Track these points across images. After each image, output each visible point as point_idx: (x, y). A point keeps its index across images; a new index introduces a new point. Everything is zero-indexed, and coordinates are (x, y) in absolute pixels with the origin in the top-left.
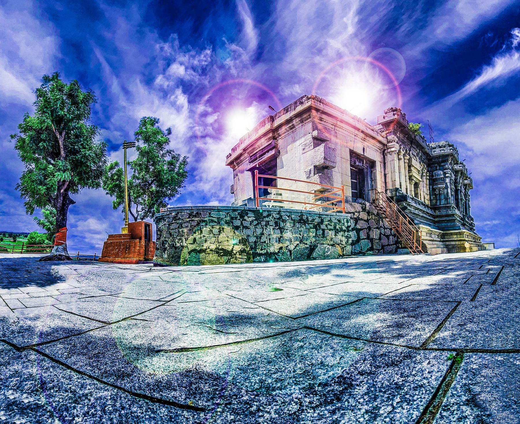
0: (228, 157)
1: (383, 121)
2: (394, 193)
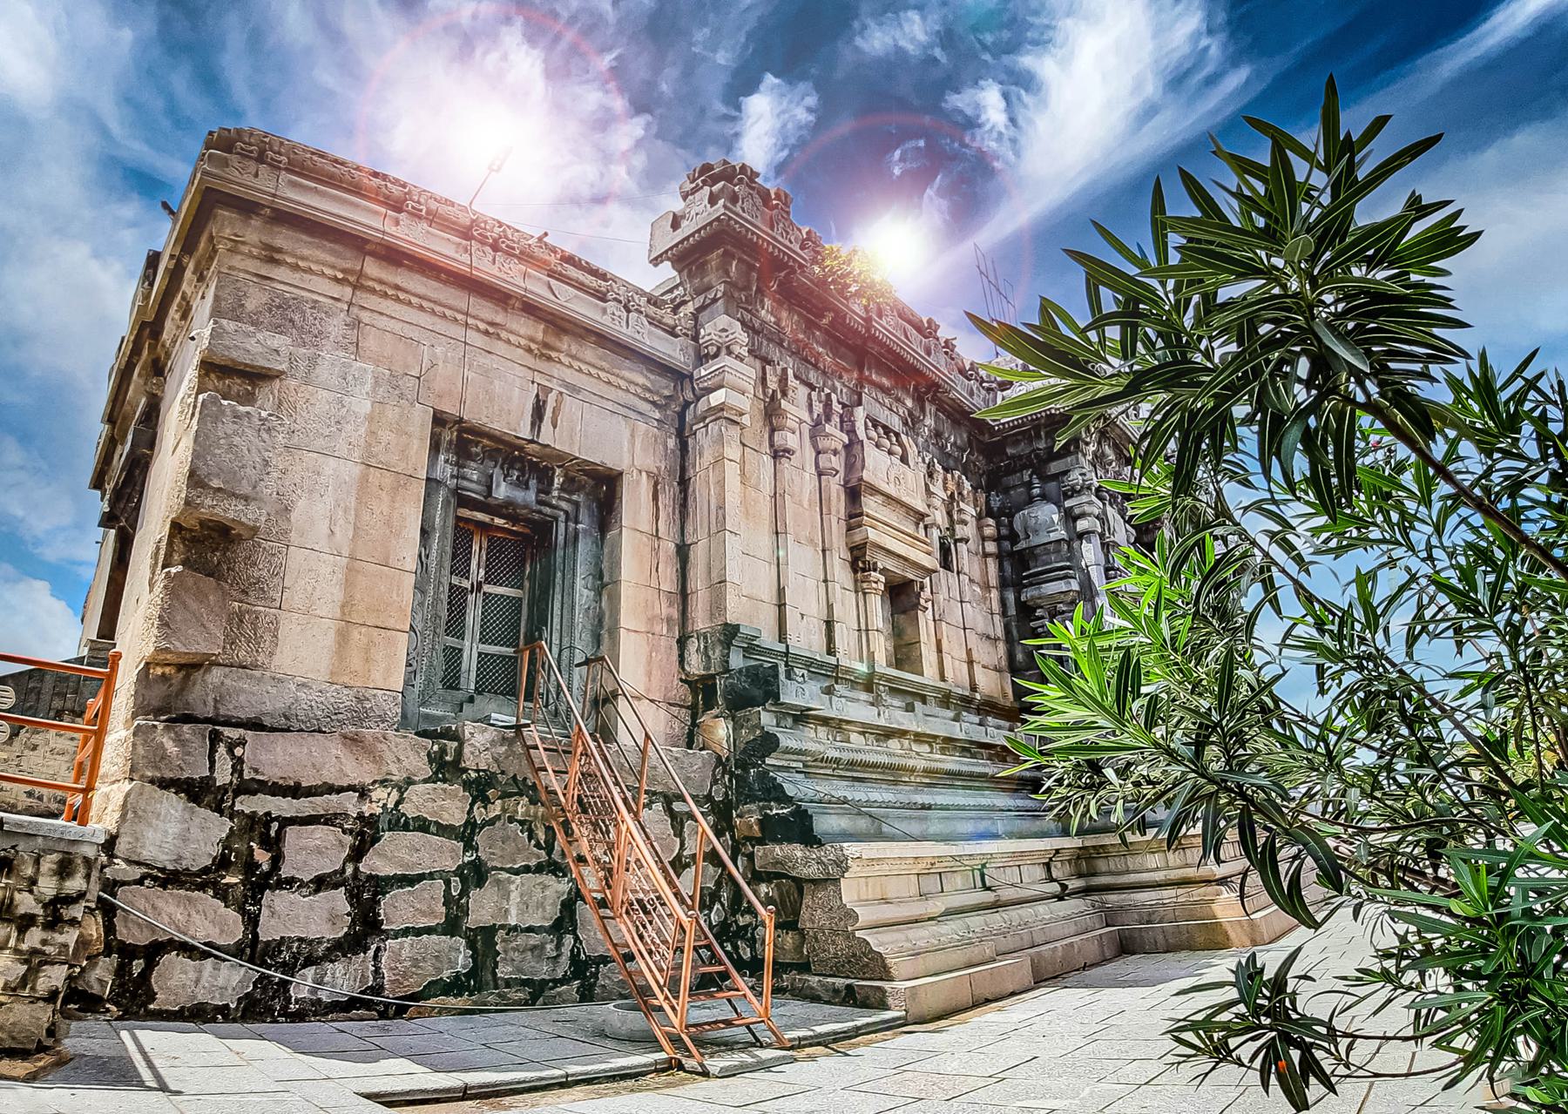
0: (98, 483)
1: (671, 239)
2: (716, 655)
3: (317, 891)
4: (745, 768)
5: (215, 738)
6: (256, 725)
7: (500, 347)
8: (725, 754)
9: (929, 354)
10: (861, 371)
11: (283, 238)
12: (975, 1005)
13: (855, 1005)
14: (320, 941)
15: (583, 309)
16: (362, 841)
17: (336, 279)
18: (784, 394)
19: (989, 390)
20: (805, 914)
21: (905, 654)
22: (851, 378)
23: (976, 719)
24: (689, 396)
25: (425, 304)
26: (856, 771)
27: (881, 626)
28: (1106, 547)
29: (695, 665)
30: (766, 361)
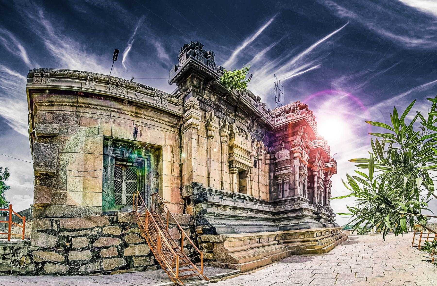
3: (82, 250)
4: (198, 218)
5: (52, 221)
6: (64, 217)
7: (122, 116)
8: (193, 215)
9: (257, 107)
10: (235, 113)
11: (54, 98)
12: (258, 268)
13: (228, 268)
14: (85, 260)
15: (147, 100)
16: (93, 240)
17: (71, 106)
18: (211, 120)
19: (273, 117)
20: (214, 250)
21: (242, 188)
22: (232, 116)
23: (260, 205)
24: (182, 123)
25: (98, 107)
26: (229, 217)
27: (236, 182)
28: (301, 161)
29: (185, 194)
30: (206, 111)
